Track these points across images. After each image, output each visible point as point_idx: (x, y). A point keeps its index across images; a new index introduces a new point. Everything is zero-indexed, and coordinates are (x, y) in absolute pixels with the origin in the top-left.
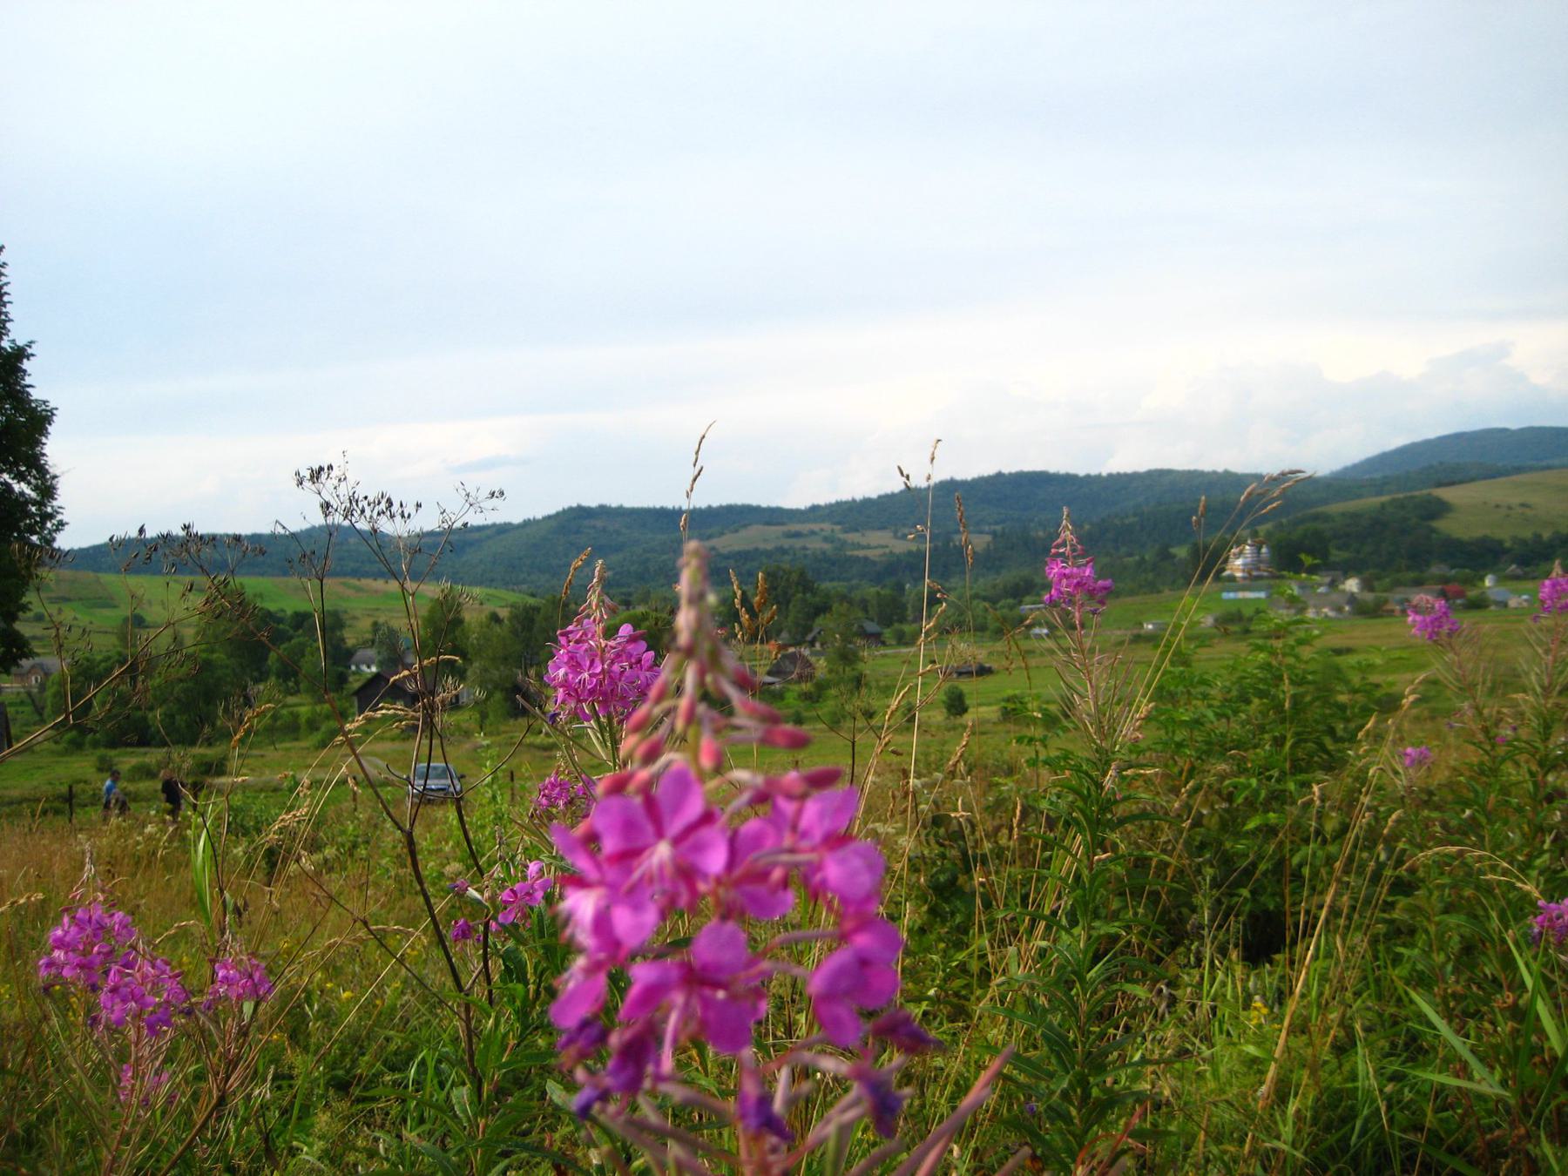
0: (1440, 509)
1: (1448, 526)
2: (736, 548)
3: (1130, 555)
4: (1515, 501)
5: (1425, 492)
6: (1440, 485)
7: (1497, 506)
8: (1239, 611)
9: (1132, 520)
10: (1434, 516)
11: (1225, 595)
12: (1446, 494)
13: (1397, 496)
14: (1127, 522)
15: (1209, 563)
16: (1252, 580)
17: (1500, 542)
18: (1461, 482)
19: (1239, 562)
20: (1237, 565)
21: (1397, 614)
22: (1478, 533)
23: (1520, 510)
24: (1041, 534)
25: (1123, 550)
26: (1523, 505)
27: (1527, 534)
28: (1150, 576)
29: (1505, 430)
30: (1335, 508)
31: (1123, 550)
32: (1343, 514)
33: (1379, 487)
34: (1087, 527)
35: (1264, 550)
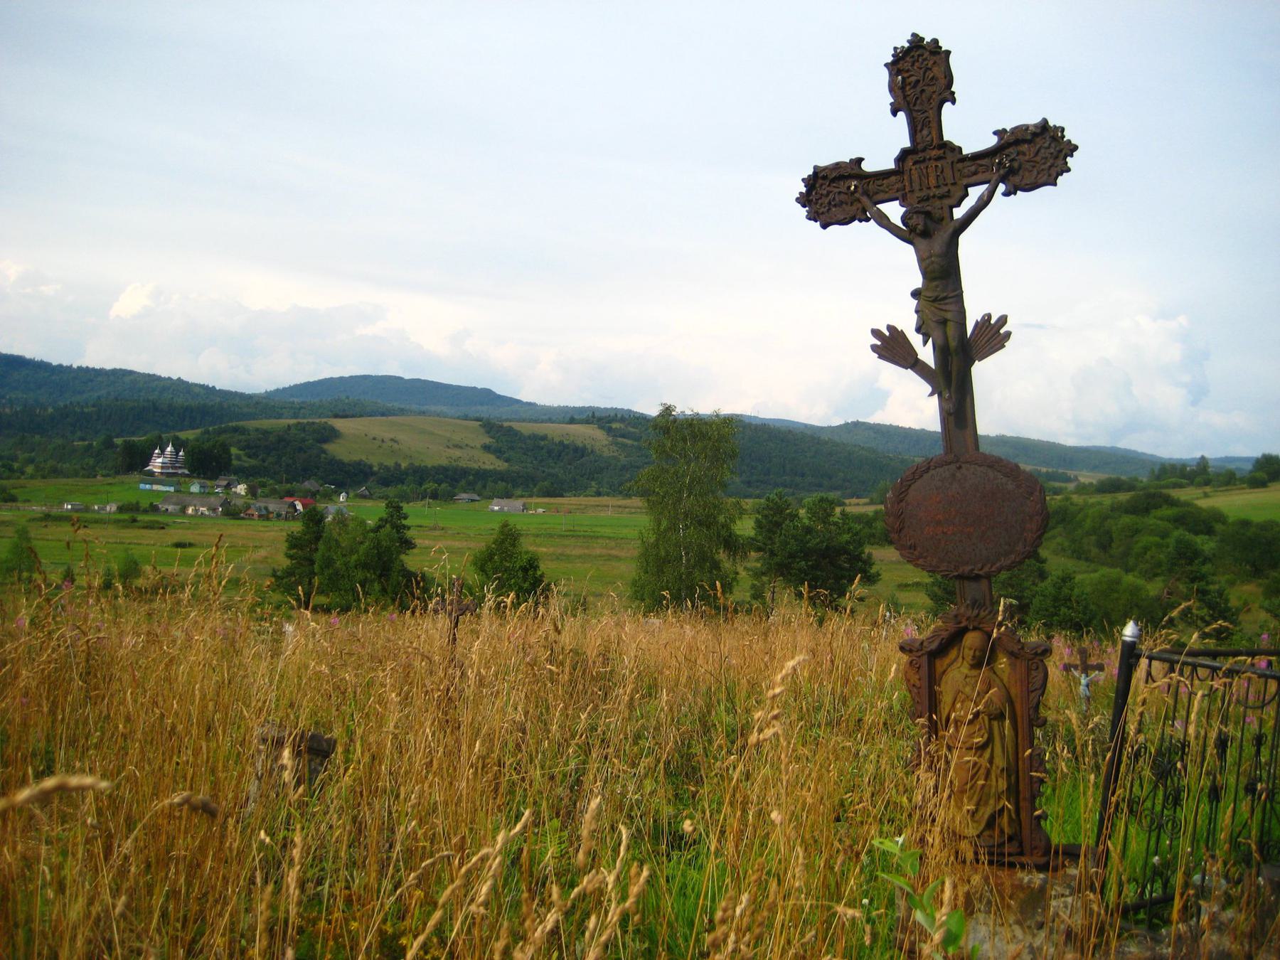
0: (331, 435)
1: (336, 450)
2: (265, 427)
3: (83, 439)
4: (387, 436)
5: (324, 420)
6: (336, 416)
7: (374, 439)
8: (138, 503)
9: (91, 409)
10: (325, 440)
11: (142, 486)
12: (339, 424)
13: (301, 421)
14: (86, 410)
15: (136, 460)
16: (167, 477)
17: (371, 467)
18: (353, 416)
19: (160, 460)
20: (157, 464)
21: (256, 517)
22: (356, 457)
23: (390, 444)
24: (7, 410)
25: (79, 434)
26: (392, 440)
27: (390, 463)
28: (91, 461)
29: (401, 379)
30: (252, 424)
31: (79, 434)
32: (257, 430)
33: (296, 411)
34: (50, 410)
35: (181, 453)
